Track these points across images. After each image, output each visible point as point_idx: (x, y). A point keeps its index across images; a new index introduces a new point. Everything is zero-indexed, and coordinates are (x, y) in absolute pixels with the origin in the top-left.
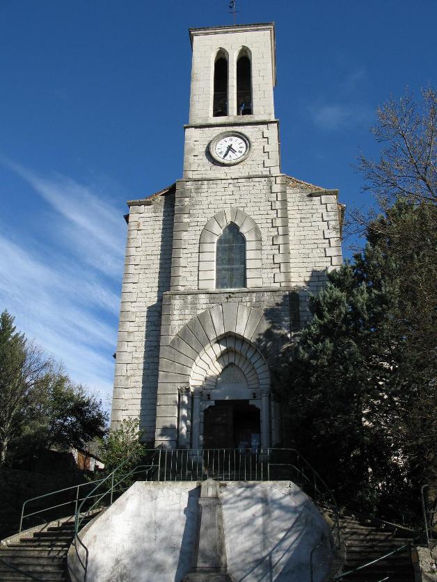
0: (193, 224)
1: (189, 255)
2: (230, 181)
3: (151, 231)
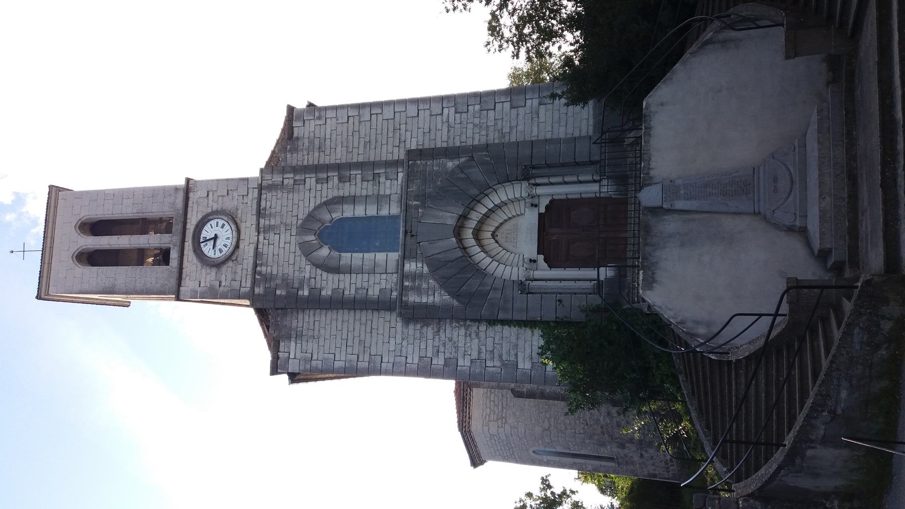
2: (261, 237)
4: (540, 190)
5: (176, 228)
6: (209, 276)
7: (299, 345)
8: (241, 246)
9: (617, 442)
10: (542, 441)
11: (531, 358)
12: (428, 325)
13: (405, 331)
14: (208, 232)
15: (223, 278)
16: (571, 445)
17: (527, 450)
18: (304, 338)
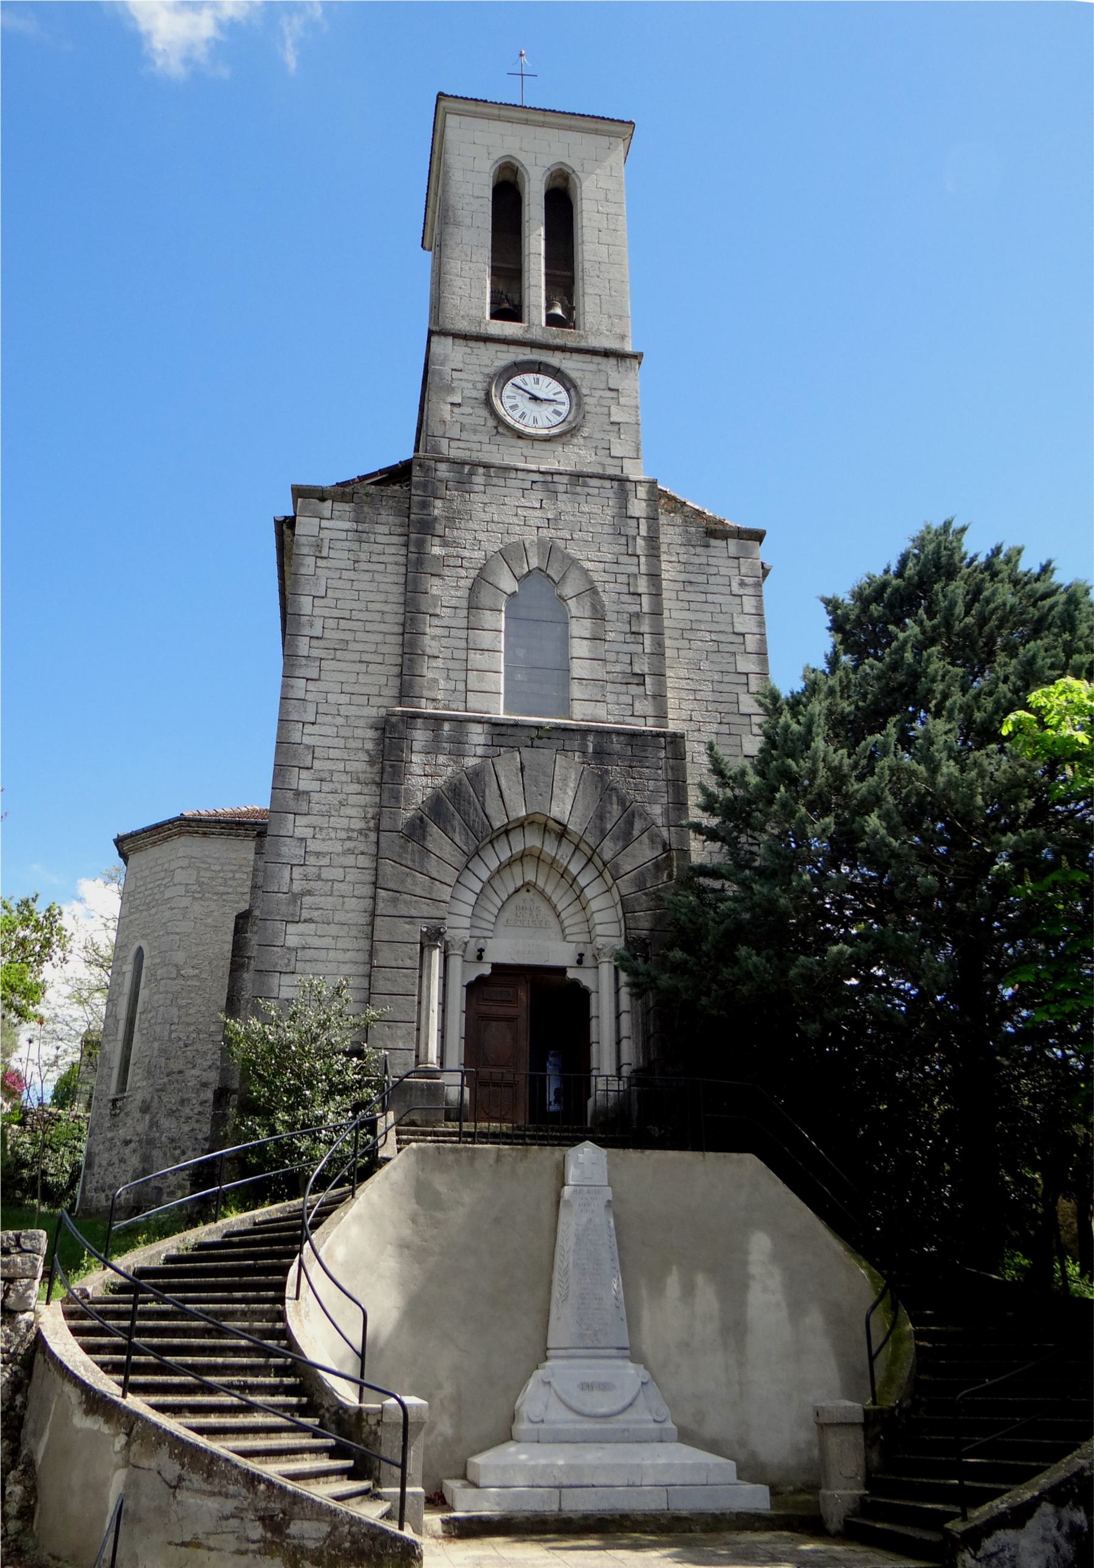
0: (452, 562)
1: (374, 558)
3: (349, 564)
4: (606, 970)
5: (557, 336)
6: (470, 385)
7: (343, 535)
8: (521, 443)
9: (152, 1098)
10: (158, 964)
11: (304, 948)
12: (371, 763)
13: (362, 723)
14: (546, 386)
15: (466, 410)
16: (150, 1016)
17: (144, 936)
18: (355, 546)
